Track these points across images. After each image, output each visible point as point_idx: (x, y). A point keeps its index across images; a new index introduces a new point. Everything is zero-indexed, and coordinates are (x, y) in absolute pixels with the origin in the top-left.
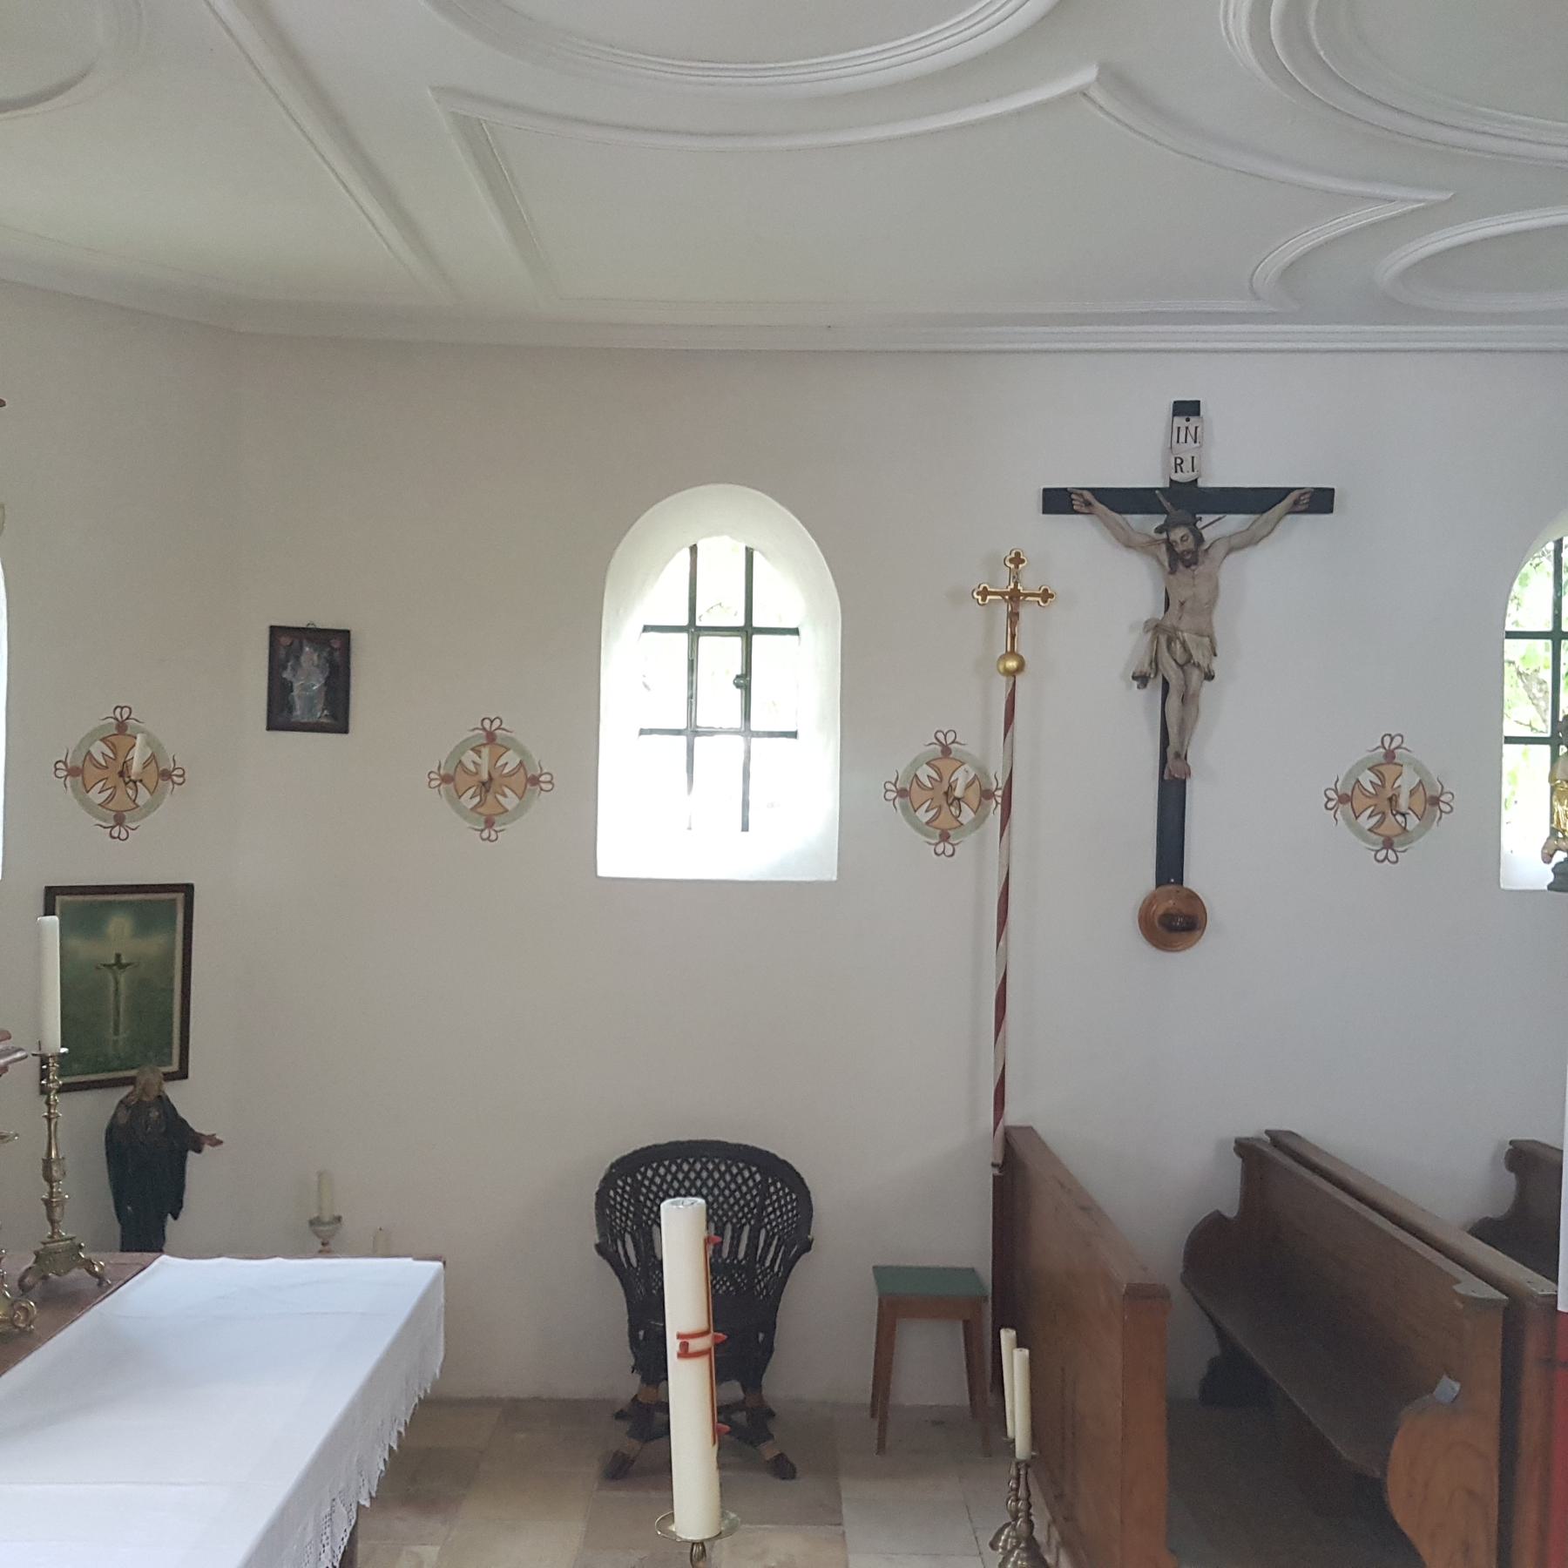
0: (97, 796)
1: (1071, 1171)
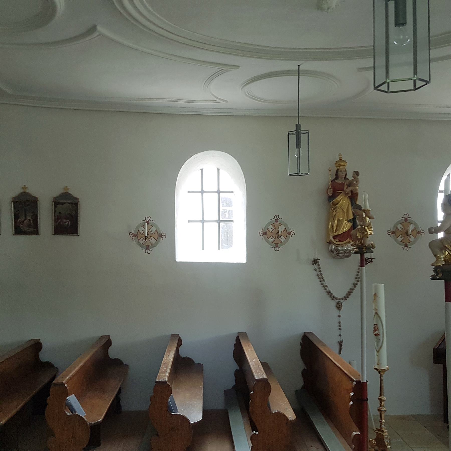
0: (399, 239)
1: (39, 356)
